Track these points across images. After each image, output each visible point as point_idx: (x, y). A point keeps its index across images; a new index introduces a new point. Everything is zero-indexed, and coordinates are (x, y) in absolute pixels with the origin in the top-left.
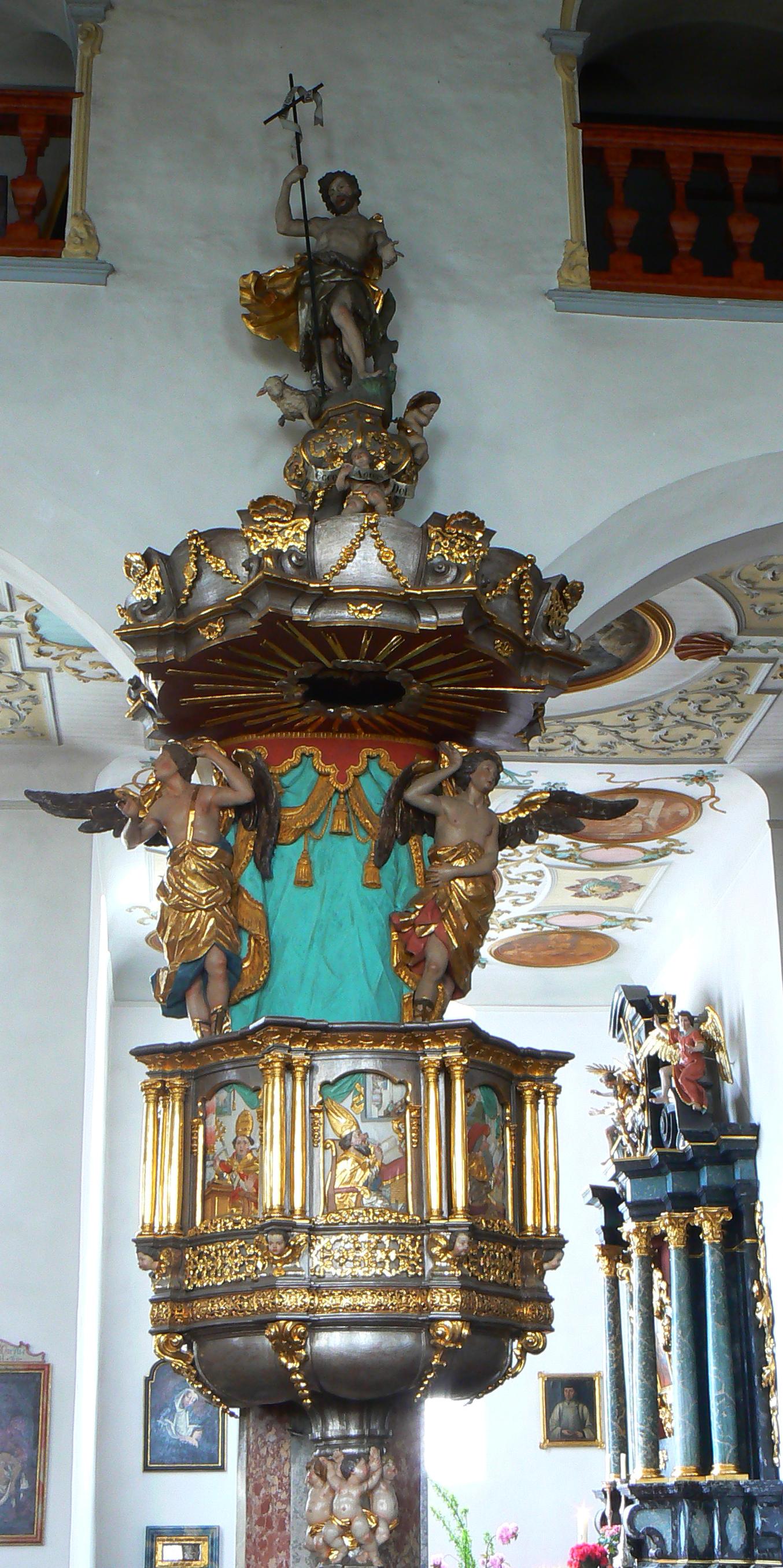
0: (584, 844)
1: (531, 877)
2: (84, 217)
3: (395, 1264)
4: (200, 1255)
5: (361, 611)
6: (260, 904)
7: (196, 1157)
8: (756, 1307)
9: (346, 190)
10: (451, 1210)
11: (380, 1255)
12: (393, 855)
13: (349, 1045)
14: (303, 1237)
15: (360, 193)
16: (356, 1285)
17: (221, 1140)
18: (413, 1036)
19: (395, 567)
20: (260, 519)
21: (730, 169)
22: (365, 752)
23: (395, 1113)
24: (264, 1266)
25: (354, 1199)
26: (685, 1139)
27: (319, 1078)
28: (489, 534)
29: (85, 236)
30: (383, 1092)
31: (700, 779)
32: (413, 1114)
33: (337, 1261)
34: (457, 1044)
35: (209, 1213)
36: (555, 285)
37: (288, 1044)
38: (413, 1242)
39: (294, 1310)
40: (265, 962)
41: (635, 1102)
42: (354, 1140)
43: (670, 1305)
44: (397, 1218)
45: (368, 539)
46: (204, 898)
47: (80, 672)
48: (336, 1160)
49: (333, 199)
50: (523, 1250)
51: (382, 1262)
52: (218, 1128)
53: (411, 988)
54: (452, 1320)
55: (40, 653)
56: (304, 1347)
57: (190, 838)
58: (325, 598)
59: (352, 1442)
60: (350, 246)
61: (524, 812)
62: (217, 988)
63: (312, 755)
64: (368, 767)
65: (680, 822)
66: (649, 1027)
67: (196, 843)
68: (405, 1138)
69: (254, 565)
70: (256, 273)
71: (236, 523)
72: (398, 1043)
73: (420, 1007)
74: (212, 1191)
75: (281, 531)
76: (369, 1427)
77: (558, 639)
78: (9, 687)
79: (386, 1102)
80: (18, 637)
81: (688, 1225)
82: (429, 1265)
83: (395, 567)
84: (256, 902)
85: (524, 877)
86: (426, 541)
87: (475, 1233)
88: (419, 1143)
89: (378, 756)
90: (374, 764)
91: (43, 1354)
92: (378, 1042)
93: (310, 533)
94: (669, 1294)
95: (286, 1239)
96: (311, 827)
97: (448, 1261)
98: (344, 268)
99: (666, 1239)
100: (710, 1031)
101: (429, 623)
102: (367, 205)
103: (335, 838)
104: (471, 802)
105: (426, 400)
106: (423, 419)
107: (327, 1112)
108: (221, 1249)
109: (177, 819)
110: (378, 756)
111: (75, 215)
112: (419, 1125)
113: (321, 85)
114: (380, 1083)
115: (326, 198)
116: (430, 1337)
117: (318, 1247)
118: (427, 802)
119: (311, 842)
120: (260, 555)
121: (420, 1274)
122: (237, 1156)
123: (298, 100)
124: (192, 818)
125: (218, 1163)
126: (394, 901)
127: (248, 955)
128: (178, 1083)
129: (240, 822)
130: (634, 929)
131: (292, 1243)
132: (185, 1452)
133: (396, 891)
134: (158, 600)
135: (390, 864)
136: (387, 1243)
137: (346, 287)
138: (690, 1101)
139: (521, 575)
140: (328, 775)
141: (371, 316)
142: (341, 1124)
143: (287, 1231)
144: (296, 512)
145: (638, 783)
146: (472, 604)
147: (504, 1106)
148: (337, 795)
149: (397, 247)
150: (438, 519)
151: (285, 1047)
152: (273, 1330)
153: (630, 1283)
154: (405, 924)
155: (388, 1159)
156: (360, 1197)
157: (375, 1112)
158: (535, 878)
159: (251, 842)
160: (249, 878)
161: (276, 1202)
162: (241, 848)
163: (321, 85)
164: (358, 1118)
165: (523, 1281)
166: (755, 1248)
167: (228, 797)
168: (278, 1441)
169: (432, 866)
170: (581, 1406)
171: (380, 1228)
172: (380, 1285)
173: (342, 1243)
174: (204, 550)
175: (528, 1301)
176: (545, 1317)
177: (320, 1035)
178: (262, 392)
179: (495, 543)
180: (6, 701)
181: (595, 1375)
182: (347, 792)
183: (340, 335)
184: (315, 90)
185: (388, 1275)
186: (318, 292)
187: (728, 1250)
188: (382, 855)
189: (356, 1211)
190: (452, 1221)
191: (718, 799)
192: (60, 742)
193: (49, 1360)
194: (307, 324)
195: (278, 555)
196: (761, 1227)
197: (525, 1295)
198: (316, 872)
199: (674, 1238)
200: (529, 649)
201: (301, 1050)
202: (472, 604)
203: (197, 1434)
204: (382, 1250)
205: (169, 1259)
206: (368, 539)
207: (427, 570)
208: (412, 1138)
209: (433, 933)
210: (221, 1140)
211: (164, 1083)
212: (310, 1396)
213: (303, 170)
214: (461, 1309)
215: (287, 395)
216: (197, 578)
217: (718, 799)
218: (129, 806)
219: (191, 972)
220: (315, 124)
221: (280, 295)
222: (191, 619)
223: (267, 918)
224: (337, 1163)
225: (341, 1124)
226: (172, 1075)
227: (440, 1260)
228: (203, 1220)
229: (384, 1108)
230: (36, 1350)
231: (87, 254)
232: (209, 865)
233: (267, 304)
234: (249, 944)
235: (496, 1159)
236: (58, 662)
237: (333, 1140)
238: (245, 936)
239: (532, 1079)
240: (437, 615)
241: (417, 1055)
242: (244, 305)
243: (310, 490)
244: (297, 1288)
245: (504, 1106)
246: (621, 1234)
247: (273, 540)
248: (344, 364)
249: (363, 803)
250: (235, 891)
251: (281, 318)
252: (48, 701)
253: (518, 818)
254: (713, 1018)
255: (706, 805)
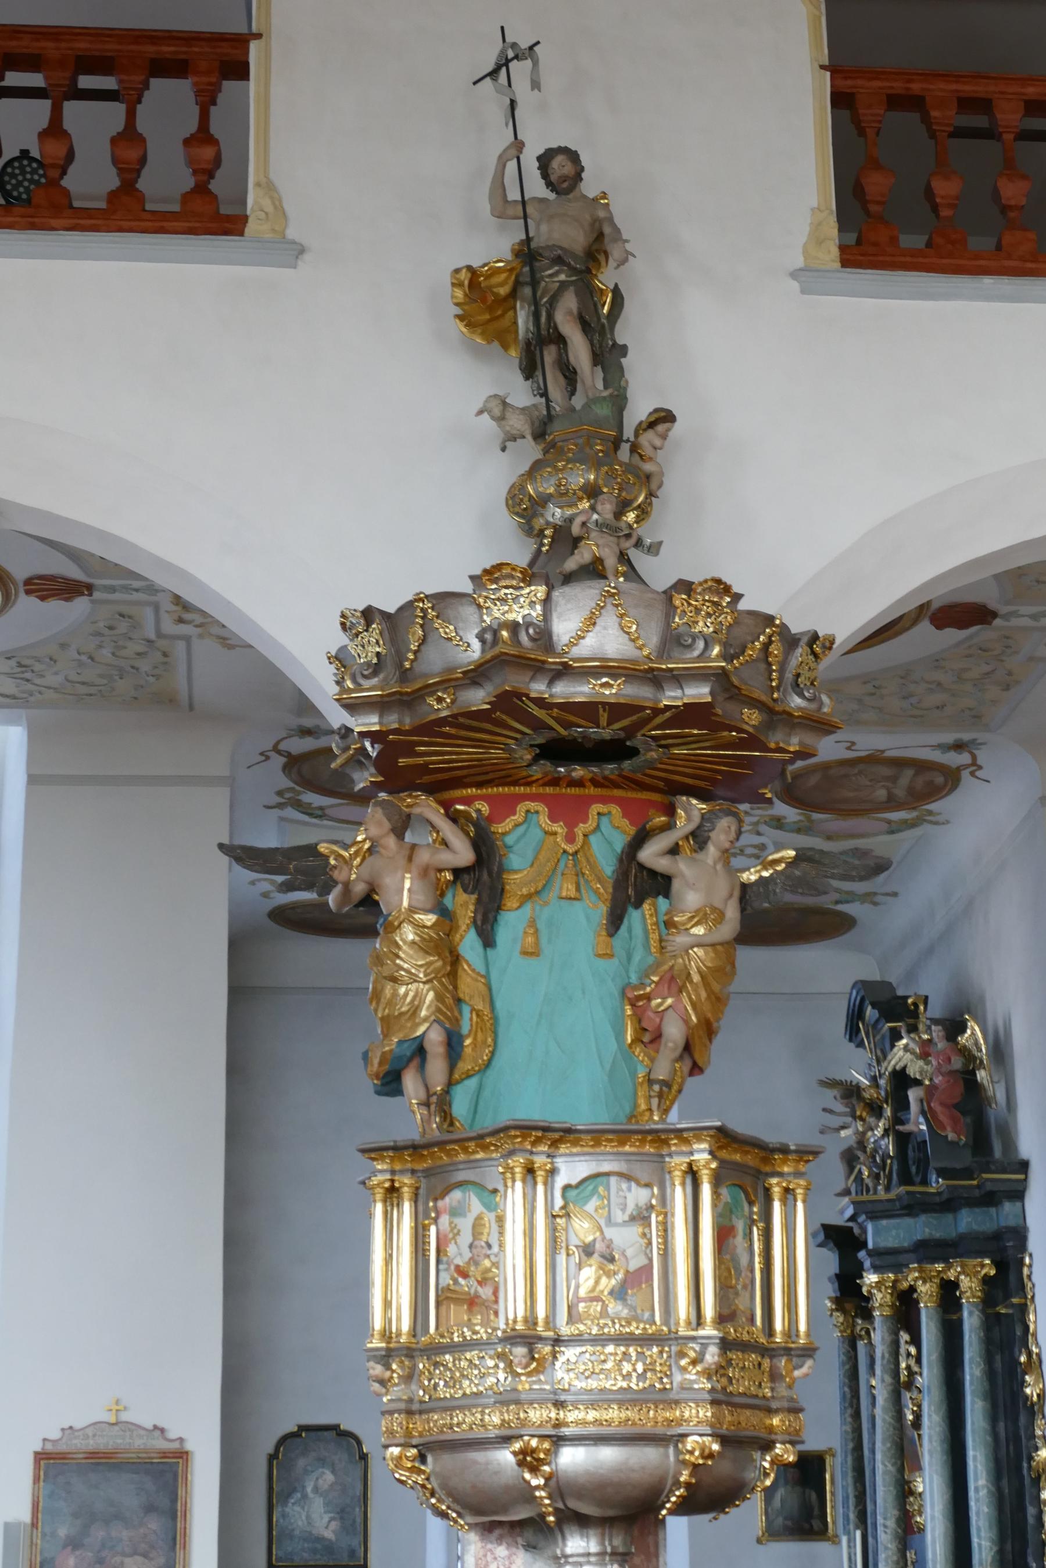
0: (816, 816)
1: (749, 851)
2: (269, 187)
3: (642, 1377)
4: (436, 1364)
5: (603, 685)
6: (482, 976)
7: (428, 1260)
8: (1024, 1381)
9: (569, 169)
10: (700, 1322)
11: (627, 1367)
12: (626, 921)
13: (592, 1146)
14: (548, 1349)
15: (582, 169)
16: (599, 1399)
17: (456, 1243)
18: (659, 1137)
19: (638, 638)
20: (494, 586)
21: (999, 116)
22: (595, 808)
23: (641, 1217)
24: (506, 1378)
25: (599, 1308)
26: (939, 1176)
27: (560, 1181)
28: (737, 597)
29: (270, 209)
30: (628, 1195)
31: (959, 746)
32: (660, 1218)
33: (582, 1373)
34: (704, 1146)
35: (443, 1320)
36: (799, 262)
37: (529, 1147)
38: (661, 1352)
39: (540, 1426)
40: (490, 1040)
41: (877, 1126)
42: (599, 1246)
43: (921, 1374)
44: (645, 1329)
45: (609, 607)
46: (422, 970)
47: (225, 639)
48: (580, 1266)
49: (553, 178)
50: (771, 1357)
51: (629, 1374)
52: (452, 1230)
53: (647, 1066)
54: (701, 1435)
55: (181, 621)
56: (549, 1464)
57: (405, 903)
58: (564, 671)
59: (593, 1559)
60: (572, 237)
61: (767, 870)
62: (437, 1068)
63: (537, 812)
64: (598, 826)
65: (934, 792)
66: (896, 1036)
67: (412, 910)
68: (650, 1243)
69: (488, 636)
70: (469, 268)
71: (467, 587)
72: (643, 1142)
73: (656, 1088)
74: (447, 1298)
75: (515, 599)
76: (610, 1541)
77: (808, 700)
78: (139, 654)
79: (631, 1208)
80: (157, 608)
81: (942, 1279)
82: (678, 1378)
83: (638, 638)
84: (478, 974)
85: (742, 851)
86: (670, 609)
87: (726, 1345)
88: (666, 1250)
89: (610, 813)
90: (605, 820)
91: (181, 1440)
92: (622, 1143)
93: (547, 601)
94: (919, 1360)
95: (531, 1351)
96: (537, 893)
97: (698, 1373)
98: (569, 265)
99: (915, 1296)
100: (970, 1044)
101: (675, 698)
102: (589, 187)
103: (563, 903)
104: (710, 861)
105: (663, 418)
106: (658, 442)
107: (569, 1216)
108: (460, 1360)
109: (388, 881)
110: (610, 813)
111: (258, 184)
112: (665, 1230)
113: (538, 43)
114: (624, 1186)
115: (545, 175)
116: (678, 1452)
117: (562, 1359)
118: (662, 864)
119: (538, 908)
120: (495, 627)
121: (668, 1386)
122: (474, 1261)
123: (512, 59)
124: (407, 884)
125: (452, 1267)
126: (627, 972)
127: (470, 1031)
128: (406, 1181)
129: (459, 885)
130: (875, 904)
131: (536, 1356)
132: (319, 1546)
133: (629, 958)
134: (379, 660)
135: (624, 928)
136: (634, 1354)
137: (572, 288)
138: (944, 1128)
139: (770, 637)
140: (555, 834)
141: (599, 319)
142: (582, 1229)
143: (532, 1343)
144: (529, 577)
145: (883, 751)
146: (721, 679)
147: (751, 1203)
148: (565, 856)
149: (628, 246)
150: (685, 587)
151: (526, 1151)
152: (517, 1446)
153: (870, 1343)
154: (639, 998)
155: (633, 1266)
156: (605, 1307)
157: (619, 1216)
158: (756, 851)
159: (472, 907)
160: (469, 944)
161: (521, 1314)
162: (460, 912)
163: (538, 43)
164: (602, 1222)
165: (772, 1389)
166: (1023, 1309)
167: (448, 859)
168: (509, 1557)
169: (668, 934)
170: (807, 1491)
171: (626, 1339)
172: (626, 1399)
173: (587, 1355)
174: (431, 613)
175: (777, 1411)
176: (796, 1430)
177: (560, 1136)
178: (480, 412)
179: (743, 605)
180: (133, 667)
181: (826, 1452)
182: (576, 853)
183: (565, 343)
184: (531, 48)
185: (635, 1387)
186: (539, 294)
187: (990, 1311)
188: (615, 920)
189: (602, 1322)
190: (701, 1332)
191: (980, 768)
192: (191, 707)
193: (189, 1446)
194: (527, 330)
195: (514, 627)
196: (1030, 1285)
197: (774, 1405)
198: (544, 941)
199: (926, 1291)
200: (778, 713)
201: (543, 1153)
202: (721, 679)
203: (334, 1525)
204: (629, 1361)
205: (402, 1368)
206: (609, 607)
207: (674, 640)
208: (658, 1243)
209: (670, 1006)
210: (456, 1243)
211: (392, 1181)
212: (554, 1515)
213: (518, 145)
214: (712, 1426)
215: (508, 415)
216: (424, 641)
217: (980, 768)
218: (340, 872)
219: (408, 1050)
220: (532, 89)
221: (496, 295)
222: (417, 686)
223: (490, 989)
224: (580, 1269)
225: (582, 1229)
226: (402, 1172)
227: (689, 1373)
228: (437, 1328)
229: (629, 1211)
230: (172, 1435)
231: (273, 230)
232: (428, 934)
233: (484, 304)
234: (471, 1019)
235: (744, 1261)
236: (199, 630)
237: (576, 1247)
238: (466, 1010)
239: (780, 1174)
240: (682, 688)
241: (662, 1156)
242: (457, 304)
243: (537, 527)
244: (542, 1402)
245: (751, 1203)
246: (860, 1287)
247: (506, 608)
248: (570, 375)
249: (593, 865)
250: (455, 960)
251: (498, 318)
252: (182, 669)
253: (761, 877)
254: (973, 1029)
255: (965, 774)
